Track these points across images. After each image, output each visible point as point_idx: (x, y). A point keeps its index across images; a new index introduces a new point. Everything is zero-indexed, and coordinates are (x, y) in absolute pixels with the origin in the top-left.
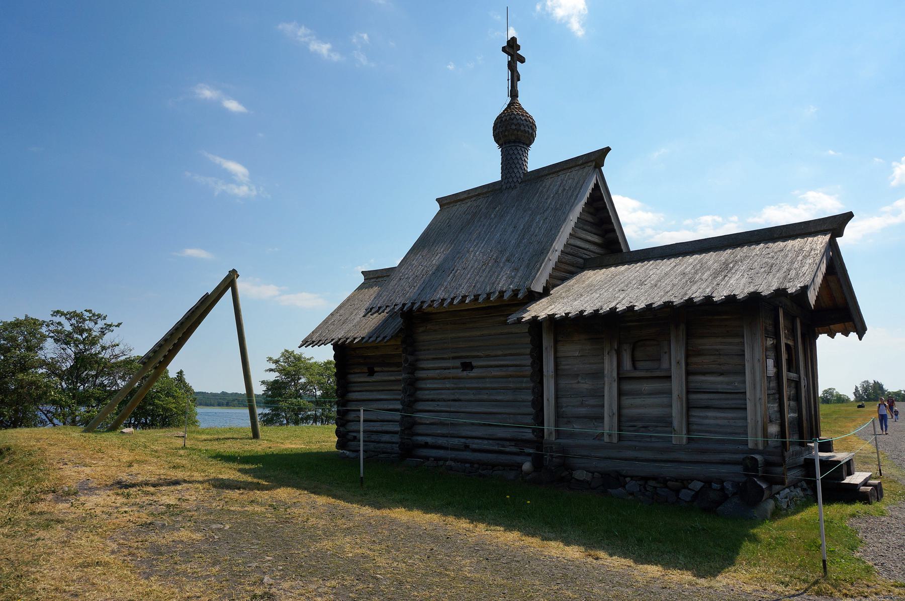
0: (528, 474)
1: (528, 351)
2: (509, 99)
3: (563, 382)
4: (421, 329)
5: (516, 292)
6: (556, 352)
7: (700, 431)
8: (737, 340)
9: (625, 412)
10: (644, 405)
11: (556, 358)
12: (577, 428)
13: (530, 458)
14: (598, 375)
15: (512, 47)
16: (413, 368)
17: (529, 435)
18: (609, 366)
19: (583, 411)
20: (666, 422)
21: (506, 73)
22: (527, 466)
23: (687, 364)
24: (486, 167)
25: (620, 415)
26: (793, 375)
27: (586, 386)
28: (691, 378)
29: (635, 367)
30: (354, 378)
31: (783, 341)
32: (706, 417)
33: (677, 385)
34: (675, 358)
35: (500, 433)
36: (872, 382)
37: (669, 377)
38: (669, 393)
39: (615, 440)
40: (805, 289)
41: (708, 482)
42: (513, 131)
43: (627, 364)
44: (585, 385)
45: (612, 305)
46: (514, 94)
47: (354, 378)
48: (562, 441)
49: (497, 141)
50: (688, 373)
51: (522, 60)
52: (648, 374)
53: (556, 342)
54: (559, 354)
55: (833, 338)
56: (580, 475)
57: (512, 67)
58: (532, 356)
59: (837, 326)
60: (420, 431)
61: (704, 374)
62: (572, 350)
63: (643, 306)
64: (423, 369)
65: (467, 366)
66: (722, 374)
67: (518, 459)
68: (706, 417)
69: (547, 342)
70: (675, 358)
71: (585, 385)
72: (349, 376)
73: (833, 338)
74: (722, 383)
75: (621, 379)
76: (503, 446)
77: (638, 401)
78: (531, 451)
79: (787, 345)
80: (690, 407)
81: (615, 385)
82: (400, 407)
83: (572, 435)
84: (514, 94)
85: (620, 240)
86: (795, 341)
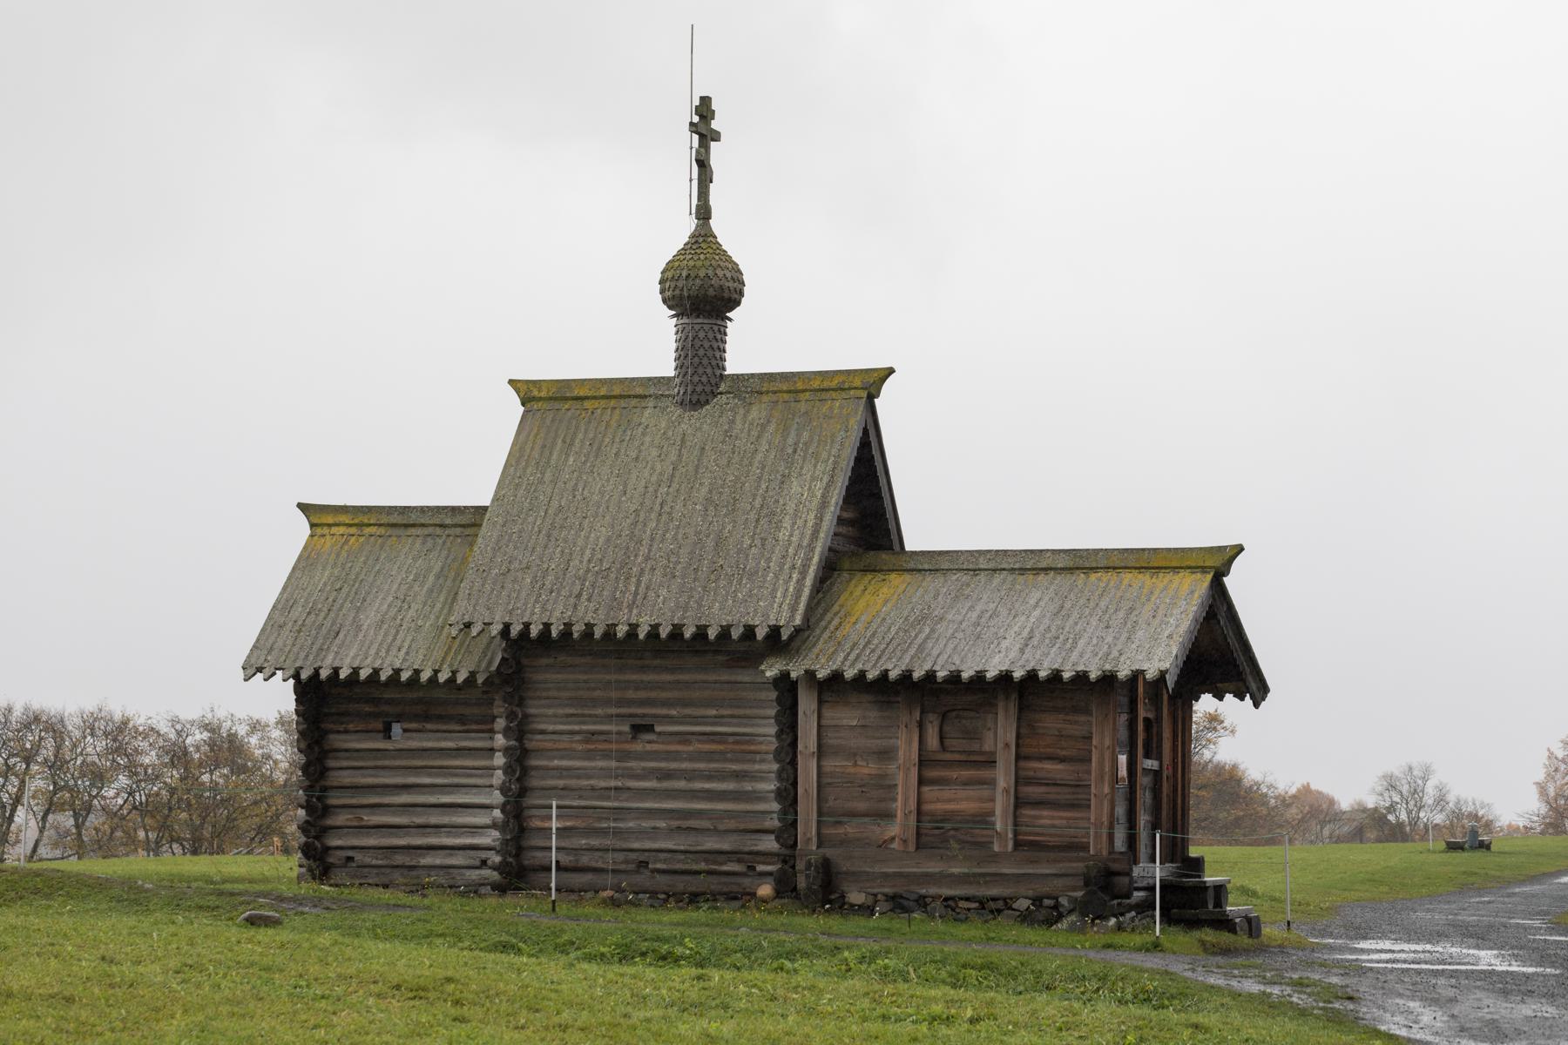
0: (764, 901)
1: (772, 712)
2: (689, 225)
3: (830, 764)
4: (545, 661)
5: (775, 631)
6: (819, 717)
7: (1030, 834)
8: (1083, 718)
9: (926, 807)
10: (954, 800)
11: (819, 726)
12: (850, 829)
13: (770, 879)
14: (886, 754)
15: (705, 110)
16: (520, 730)
17: (769, 844)
18: (906, 747)
19: (862, 806)
20: (984, 819)
21: (685, 170)
22: (765, 890)
23: (1017, 745)
24: (649, 346)
25: (919, 812)
26: (1151, 764)
27: (866, 771)
28: (1022, 764)
29: (943, 748)
30: (338, 741)
31: (1142, 713)
32: (1041, 817)
33: (1003, 777)
34: (1001, 731)
35: (711, 844)
37: (991, 763)
38: (992, 783)
39: (912, 848)
40: (1163, 674)
41: (1037, 901)
42: (703, 293)
43: (933, 741)
44: (868, 768)
45: (927, 667)
46: (704, 213)
47: (338, 741)
48: (829, 852)
50: (1018, 758)
51: (716, 136)
52: (963, 758)
53: (820, 702)
54: (824, 722)
56: (856, 897)
57: (703, 164)
58: (778, 722)
59: (1232, 686)
60: (338, 823)
61: (1040, 759)
62: (848, 716)
63: (972, 673)
64: (543, 732)
65: (639, 729)
66: (1062, 760)
67: (746, 881)
68: (1041, 817)
69: (807, 703)
70: (1001, 731)
71: (868, 768)
72: (331, 736)
75: (924, 762)
76: (715, 863)
77: (947, 793)
78: (769, 868)
79: (1146, 720)
80: (1019, 803)
81: (914, 772)
82: (497, 797)
83: (844, 842)
84: (704, 213)
85: (889, 515)
86: (1158, 710)
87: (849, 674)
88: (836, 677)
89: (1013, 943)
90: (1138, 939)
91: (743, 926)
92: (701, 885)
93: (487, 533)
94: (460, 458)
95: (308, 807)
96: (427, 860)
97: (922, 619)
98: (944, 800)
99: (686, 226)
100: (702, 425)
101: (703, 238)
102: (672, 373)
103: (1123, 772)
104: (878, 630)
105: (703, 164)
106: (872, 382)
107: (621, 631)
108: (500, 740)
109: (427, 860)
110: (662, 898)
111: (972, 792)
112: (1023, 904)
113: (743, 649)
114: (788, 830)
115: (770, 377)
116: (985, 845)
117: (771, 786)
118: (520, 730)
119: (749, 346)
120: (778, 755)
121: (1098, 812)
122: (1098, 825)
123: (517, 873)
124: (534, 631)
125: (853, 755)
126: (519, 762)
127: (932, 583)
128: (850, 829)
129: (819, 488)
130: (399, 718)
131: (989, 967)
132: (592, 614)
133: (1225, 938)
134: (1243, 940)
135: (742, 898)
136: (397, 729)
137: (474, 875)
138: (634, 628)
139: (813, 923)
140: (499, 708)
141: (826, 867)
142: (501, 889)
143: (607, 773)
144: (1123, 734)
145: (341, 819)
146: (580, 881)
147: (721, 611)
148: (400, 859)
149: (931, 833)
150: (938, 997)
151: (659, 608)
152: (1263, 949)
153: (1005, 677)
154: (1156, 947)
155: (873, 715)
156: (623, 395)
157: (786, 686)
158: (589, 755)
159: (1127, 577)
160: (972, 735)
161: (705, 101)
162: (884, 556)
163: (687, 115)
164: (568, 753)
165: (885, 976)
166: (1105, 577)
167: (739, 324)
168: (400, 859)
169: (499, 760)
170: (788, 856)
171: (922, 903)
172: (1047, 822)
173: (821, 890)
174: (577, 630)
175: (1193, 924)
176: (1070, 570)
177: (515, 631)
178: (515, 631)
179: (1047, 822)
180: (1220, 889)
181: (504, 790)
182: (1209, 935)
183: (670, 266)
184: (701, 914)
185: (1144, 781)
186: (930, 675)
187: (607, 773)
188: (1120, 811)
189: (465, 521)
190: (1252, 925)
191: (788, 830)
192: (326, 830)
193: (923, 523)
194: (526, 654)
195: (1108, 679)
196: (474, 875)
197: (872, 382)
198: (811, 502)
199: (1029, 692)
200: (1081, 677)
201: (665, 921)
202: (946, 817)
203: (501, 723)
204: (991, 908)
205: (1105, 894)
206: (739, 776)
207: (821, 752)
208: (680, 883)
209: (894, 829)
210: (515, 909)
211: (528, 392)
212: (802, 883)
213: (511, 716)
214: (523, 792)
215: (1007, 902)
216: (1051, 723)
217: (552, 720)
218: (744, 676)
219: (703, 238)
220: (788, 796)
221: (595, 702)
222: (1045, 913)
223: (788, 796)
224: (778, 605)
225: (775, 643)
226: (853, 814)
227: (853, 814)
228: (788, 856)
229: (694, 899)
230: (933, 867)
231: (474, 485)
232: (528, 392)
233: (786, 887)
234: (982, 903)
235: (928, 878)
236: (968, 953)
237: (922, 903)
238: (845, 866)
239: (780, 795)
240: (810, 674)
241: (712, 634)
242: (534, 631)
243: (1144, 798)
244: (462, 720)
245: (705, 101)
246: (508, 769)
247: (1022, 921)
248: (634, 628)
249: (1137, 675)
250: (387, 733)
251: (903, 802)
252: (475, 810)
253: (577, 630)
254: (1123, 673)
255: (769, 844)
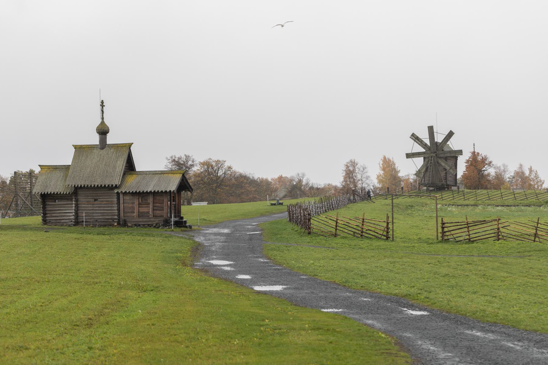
2: (101, 120)
3: (125, 205)
5: (116, 185)
10: (144, 210)
12: (128, 214)
14: (133, 203)
15: (102, 102)
17: (116, 217)
18: (136, 202)
20: (148, 212)
22: (116, 224)
24: (95, 140)
26: (174, 203)
30: (47, 203)
33: (151, 206)
34: (150, 200)
35: (107, 217)
36: (226, 165)
37: (149, 204)
38: (149, 207)
42: (103, 132)
43: (140, 201)
44: (131, 205)
46: (103, 118)
49: (98, 133)
55: (451, 131)
57: (102, 111)
62: (127, 198)
65: (95, 200)
69: (121, 196)
70: (150, 200)
73: (451, 131)
74: (227, 265)
80: (154, 210)
82: (74, 211)
83: (128, 216)
84: (103, 118)
87: (128, 192)
88: (126, 192)
89: (155, 231)
90: (170, 230)
91: (114, 230)
92: (106, 224)
93: (71, 171)
94: (66, 158)
95: (43, 213)
96: (63, 221)
97: (138, 182)
98: (142, 210)
99: (100, 121)
100: (104, 152)
101: (103, 123)
102: (98, 143)
103: (169, 205)
104: (132, 184)
105: (102, 111)
106: (130, 145)
107: (93, 186)
108: (74, 202)
109: (63, 221)
110: (100, 226)
111: (147, 208)
112: (154, 225)
113: (111, 188)
114: (119, 215)
115: (114, 144)
116: (148, 216)
117: (116, 208)
118: (77, 201)
119: (111, 139)
120: (117, 204)
121: (165, 211)
122: (165, 213)
123: (77, 222)
124: (79, 186)
125: (129, 203)
126: (77, 206)
127: (140, 176)
128: (128, 214)
129: (122, 162)
130: (57, 199)
131: (146, 234)
132: (88, 183)
133: (185, 229)
134: (189, 229)
135: (112, 225)
136: (57, 201)
137: (70, 223)
138: (94, 185)
139: (123, 229)
140: (73, 197)
141: (125, 221)
142: (74, 225)
143: (91, 207)
144: (169, 199)
145: (48, 215)
146: (88, 223)
147: (107, 183)
148: (58, 221)
149: (141, 215)
150: (139, 238)
151: (98, 182)
152: (192, 230)
153: (151, 192)
154: (173, 231)
155: (131, 197)
156: (91, 147)
157: (118, 193)
158: (88, 204)
159: (170, 175)
160: (147, 200)
161: (102, 101)
162: (133, 172)
163: (100, 103)
164: (85, 204)
165: (133, 236)
166: (166, 175)
167: (108, 136)
168: (58, 221)
169: (74, 205)
170: (119, 220)
171: (139, 225)
172: (158, 213)
173: (123, 224)
174: (86, 186)
175: (180, 227)
176: (161, 174)
177: (76, 186)
178: (76, 186)
179: (158, 213)
180: (185, 222)
181: (75, 210)
182: (183, 229)
183: (98, 127)
184: (106, 228)
185: (172, 206)
186: (140, 192)
187: (91, 207)
188: (169, 210)
189: (67, 167)
190: (190, 227)
191: (119, 215)
192: (46, 217)
193: (139, 167)
194: (77, 190)
195: (166, 192)
196: (70, 223)
197: (130, 145)
198: (121, 164)
199: (155, 194)
200: (162, 191)
201: (102, 229)
202: (143, 212)
203: (74, 200)
204: (150, 226)
205: (166, 223)
206: (111, 207)
207: (124, 203)
208: (103, 224)
209: (135, 214)
210: (78, 228)
211: (76, 147)
212: (121, 223)
213: (75, 199)
214: (78, 210)
215: (152, 225)
216: (158, 198)
217: (82, 199)
218: (112, 192)
219: (103, 123)
220: (119, 210)
221: (88, 196)
222: (157, 226)
223: (119, 210)
224: (116, 181)
225: (116, 187)
226: (129, 212)
227: (129, 212)
228: (119, 220)
229: (105, 226)
230: (141, 220)
231: (68, 161)
232: (76, 147)
233: (119, 224)
234: (149, 225)
235: (141, 221)
236: (144, 232)
237: (139, 225)
238: (128, 220)
239: (117, 210)
240: (122, 192)
241: (107, 186)
242: (79, 186)
243: (173, 208)
244: (67, 199)
245: (102, 101)
246: (75, 207)
247: (347, 174)
248: (94, 185)
249: (170, 191)
250: (55, 202)
251: (136, 211)
252: (69, 212)
253: (86, 186)
254: (168, 191)
255: (116, 217)
